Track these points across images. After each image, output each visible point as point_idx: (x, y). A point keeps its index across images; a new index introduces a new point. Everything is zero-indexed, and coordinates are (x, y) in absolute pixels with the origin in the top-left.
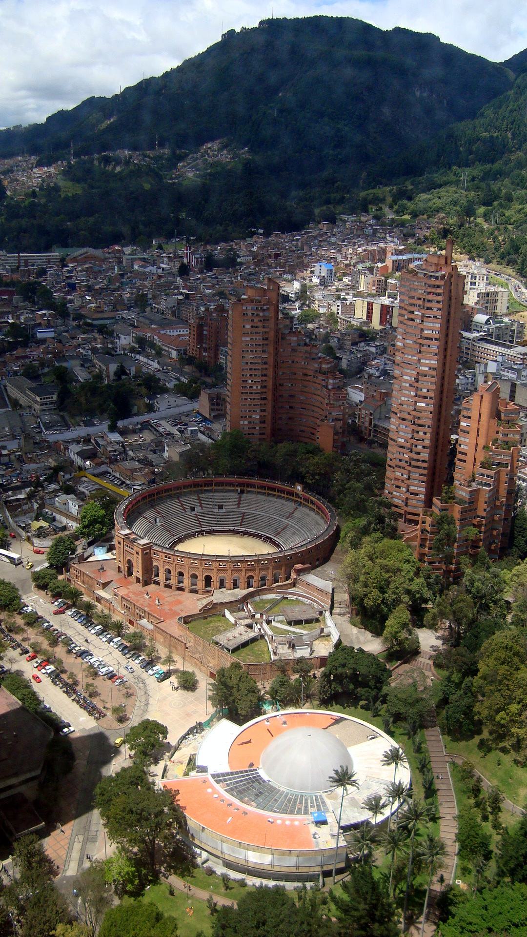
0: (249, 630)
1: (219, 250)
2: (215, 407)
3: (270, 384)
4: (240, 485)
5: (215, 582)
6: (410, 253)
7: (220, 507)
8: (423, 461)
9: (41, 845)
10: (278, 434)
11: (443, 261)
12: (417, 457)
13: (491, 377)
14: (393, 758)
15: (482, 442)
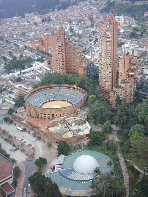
0: (65, 128)
1: (46, 16)
2: (49, 64)
3: (64, 57)
4: (59, 86)
5: (55, 116)
6: (130, 179)
7: (54, 93)
8: (109, 76)
9: (11, 158)
10: (68, 72)
11: (111, 19)
12: (108, 75)
13: (126, 49)
14: (110, 164)
15: (126, 70)
